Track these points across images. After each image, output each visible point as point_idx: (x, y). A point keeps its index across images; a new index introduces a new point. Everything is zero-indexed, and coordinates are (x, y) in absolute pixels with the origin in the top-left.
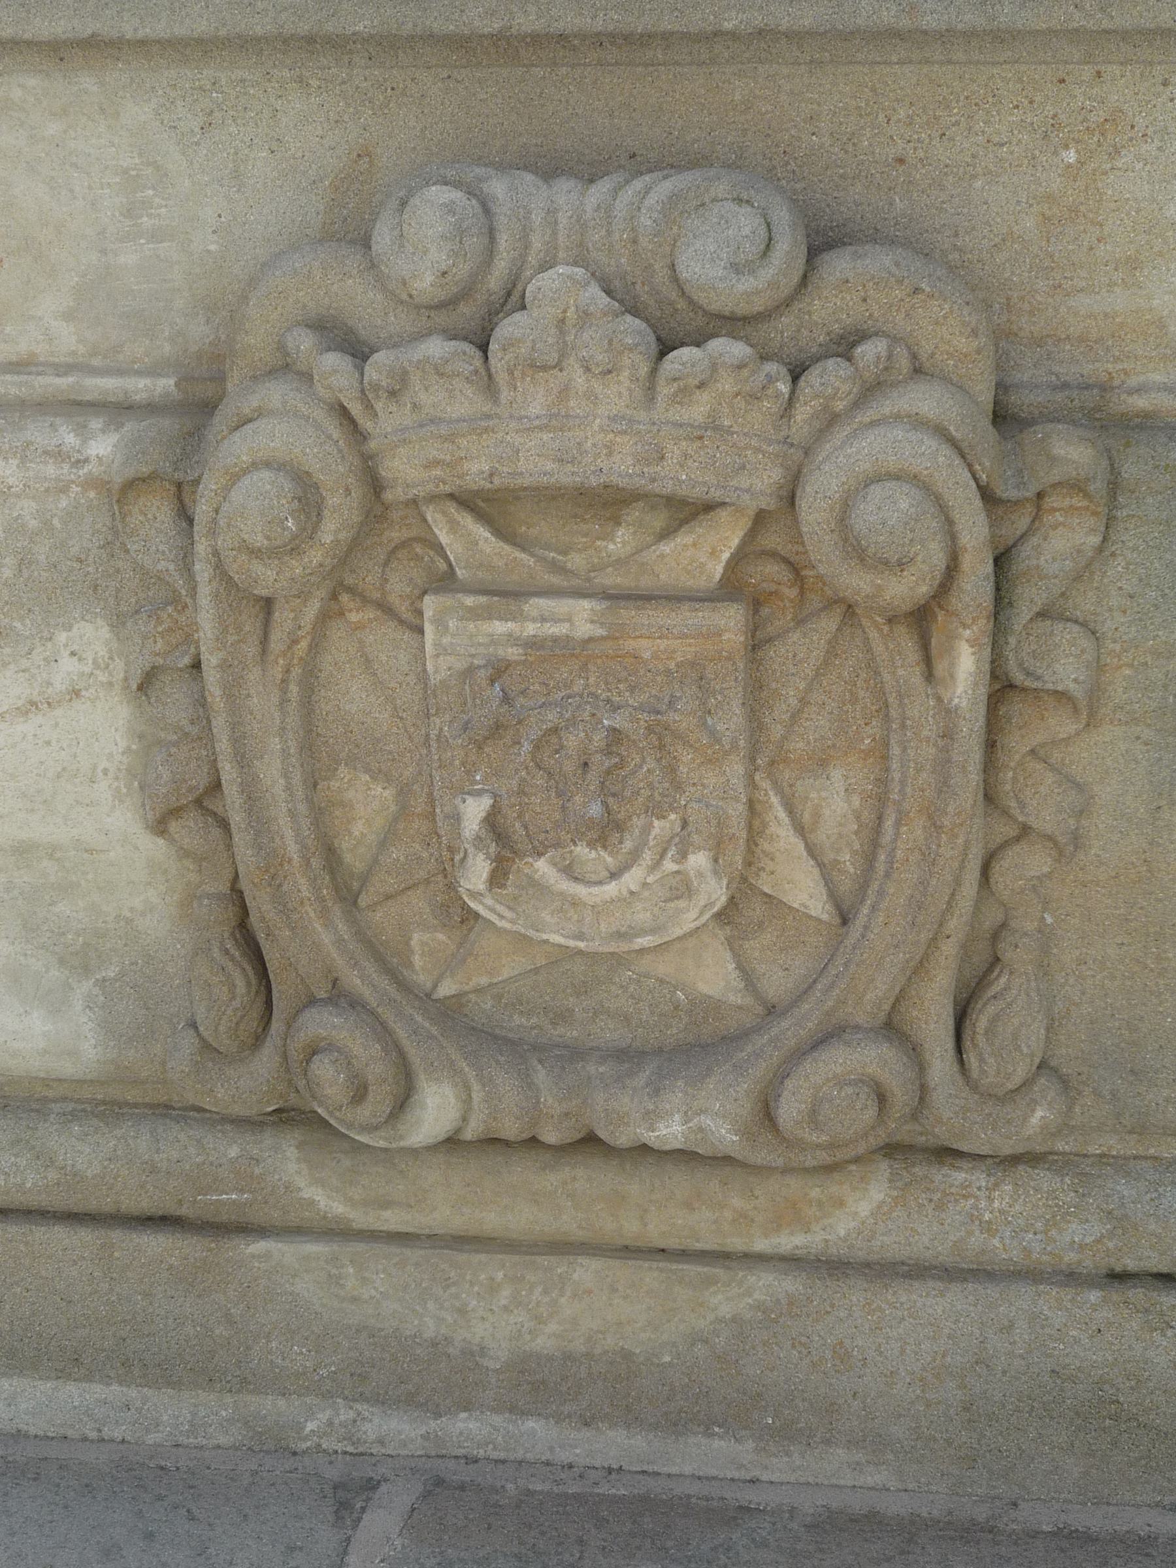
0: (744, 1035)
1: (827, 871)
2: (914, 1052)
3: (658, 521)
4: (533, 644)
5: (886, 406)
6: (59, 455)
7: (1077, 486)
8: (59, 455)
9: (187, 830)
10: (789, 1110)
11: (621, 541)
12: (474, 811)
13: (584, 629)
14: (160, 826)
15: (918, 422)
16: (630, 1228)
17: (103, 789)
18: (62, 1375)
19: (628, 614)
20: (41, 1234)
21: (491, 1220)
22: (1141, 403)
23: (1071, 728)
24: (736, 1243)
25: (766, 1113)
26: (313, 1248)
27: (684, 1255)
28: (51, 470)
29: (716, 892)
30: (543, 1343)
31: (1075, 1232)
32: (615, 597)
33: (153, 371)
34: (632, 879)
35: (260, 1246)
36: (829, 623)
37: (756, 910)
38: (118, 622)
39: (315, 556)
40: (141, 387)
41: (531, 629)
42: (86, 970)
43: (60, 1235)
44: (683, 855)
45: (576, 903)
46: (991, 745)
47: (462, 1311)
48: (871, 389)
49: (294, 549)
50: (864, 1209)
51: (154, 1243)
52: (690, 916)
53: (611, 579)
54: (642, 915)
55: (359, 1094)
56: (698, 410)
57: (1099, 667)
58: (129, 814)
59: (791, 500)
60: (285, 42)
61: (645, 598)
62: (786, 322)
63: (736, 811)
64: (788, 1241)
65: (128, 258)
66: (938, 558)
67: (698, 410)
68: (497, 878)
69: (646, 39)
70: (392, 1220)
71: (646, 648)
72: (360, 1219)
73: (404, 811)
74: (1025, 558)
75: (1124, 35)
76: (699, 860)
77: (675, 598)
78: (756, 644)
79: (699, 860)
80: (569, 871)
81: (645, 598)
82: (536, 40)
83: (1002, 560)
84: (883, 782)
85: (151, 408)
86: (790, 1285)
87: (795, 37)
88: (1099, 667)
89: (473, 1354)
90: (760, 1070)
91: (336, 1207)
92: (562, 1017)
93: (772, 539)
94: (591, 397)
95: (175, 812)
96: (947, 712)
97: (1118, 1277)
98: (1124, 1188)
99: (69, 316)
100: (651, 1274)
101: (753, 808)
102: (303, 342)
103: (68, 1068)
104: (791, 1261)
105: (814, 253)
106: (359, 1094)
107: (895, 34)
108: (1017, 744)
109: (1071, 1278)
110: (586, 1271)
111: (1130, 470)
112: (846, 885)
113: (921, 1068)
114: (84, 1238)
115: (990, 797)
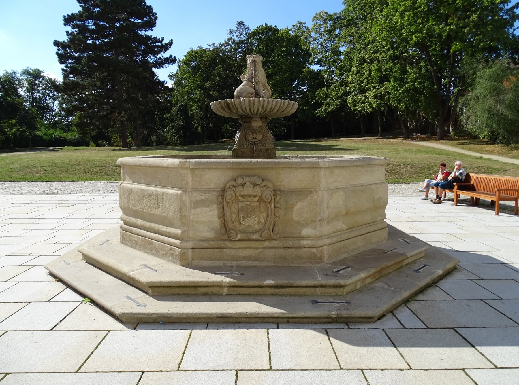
0: (259, 231)
1: (264, 219)
2: (270, 231)
3: (253, 197)
4: (245, 205)
5: (267, 190)
6: (213, 194)
7: (279, 194)
8: (213, 194)
9: (221, 219)
10: (262, 235)
11: (251, 199)
12: (242, 216)
13: (249, 204)
14: (219, 219)
15: (269, 191)
16: (251, 246)
17: (215, 217)
18: (210, 261)
19: (252, 203)
20: (208, 249)
21: (241, 246)
22: (282, 190)
23: (279, 210)
24: (258, 247)
25: (261, 236)
26: (228, 249)
27: (255, 248)
28: (213, 195)
29: (257, 221)
30: (245, 255)
31: (281, 244)
32: (251, 202)
33: (219, 189)
34: (252, 220)
35: (225, 249)
36: (264, 203)
37: (260, 222)
38: (217, 205)
39: (232, 200)
40: (219, 190)
41: (246, 204)
42: (213, 230)
43: (210, 249)
44: (255, 218)
45: (248, 222)
46: (274, 211)
47: (239, 253)
48: (266, 189)
49: (231, 199)
50: (267, 243)
51: (217, 250)
52: (256, 222)
53: (251, 201)
54: (252, 223)
55: (234, 236)
56: (256, 190)
57: (281, 206)
58: (410, 161)
59: (262, 195)
60: (229, 168)
61: (253, 202)
62: (261, 185)
63: (258, 215)
64: (262, 246)
65: (218, 181)
66: (271, 198)
67: (256, 190)
68: (243, 221)
69: (251, 168)
70: (234, 247)
71: (253, 205)
72: (232, 247)
73: (236, 216)
74: (276, 199)
75: (281, 168)
76: (256, 218)
77: (254, 202)
78: (260, 205)
79: (256, 218)
80: (248, 220)
81: (253, 202)
82: (245, 168)
83: (274, 199)
84: (268, 213)
85: (219, 191)
86: (262, 249)
87: (261, 168)
88: (281, 206)
89: (240, 256)
90: (260, 233)
91: (230, 246)
92: (247, 231)
93: (260, 198)
94: (250, 189)
95: (220, 218)
96: (271, 208)
97: (284, 248)
98: (284, 241)
99: (214, 185)
100: (252, 250)
101: (259, 216)
102: (231, 187)
103: (211, 237)
104: (261, 248)
105: (263, 181)
106: (234, 236)
107: (267, 168)
108: (276, 211)
109: (281, 248)
110: (248, 249)
111: (282, 194)
112: (265, 220)
113: (271, 233)
114: (212, 250)
115: (274, 215)
